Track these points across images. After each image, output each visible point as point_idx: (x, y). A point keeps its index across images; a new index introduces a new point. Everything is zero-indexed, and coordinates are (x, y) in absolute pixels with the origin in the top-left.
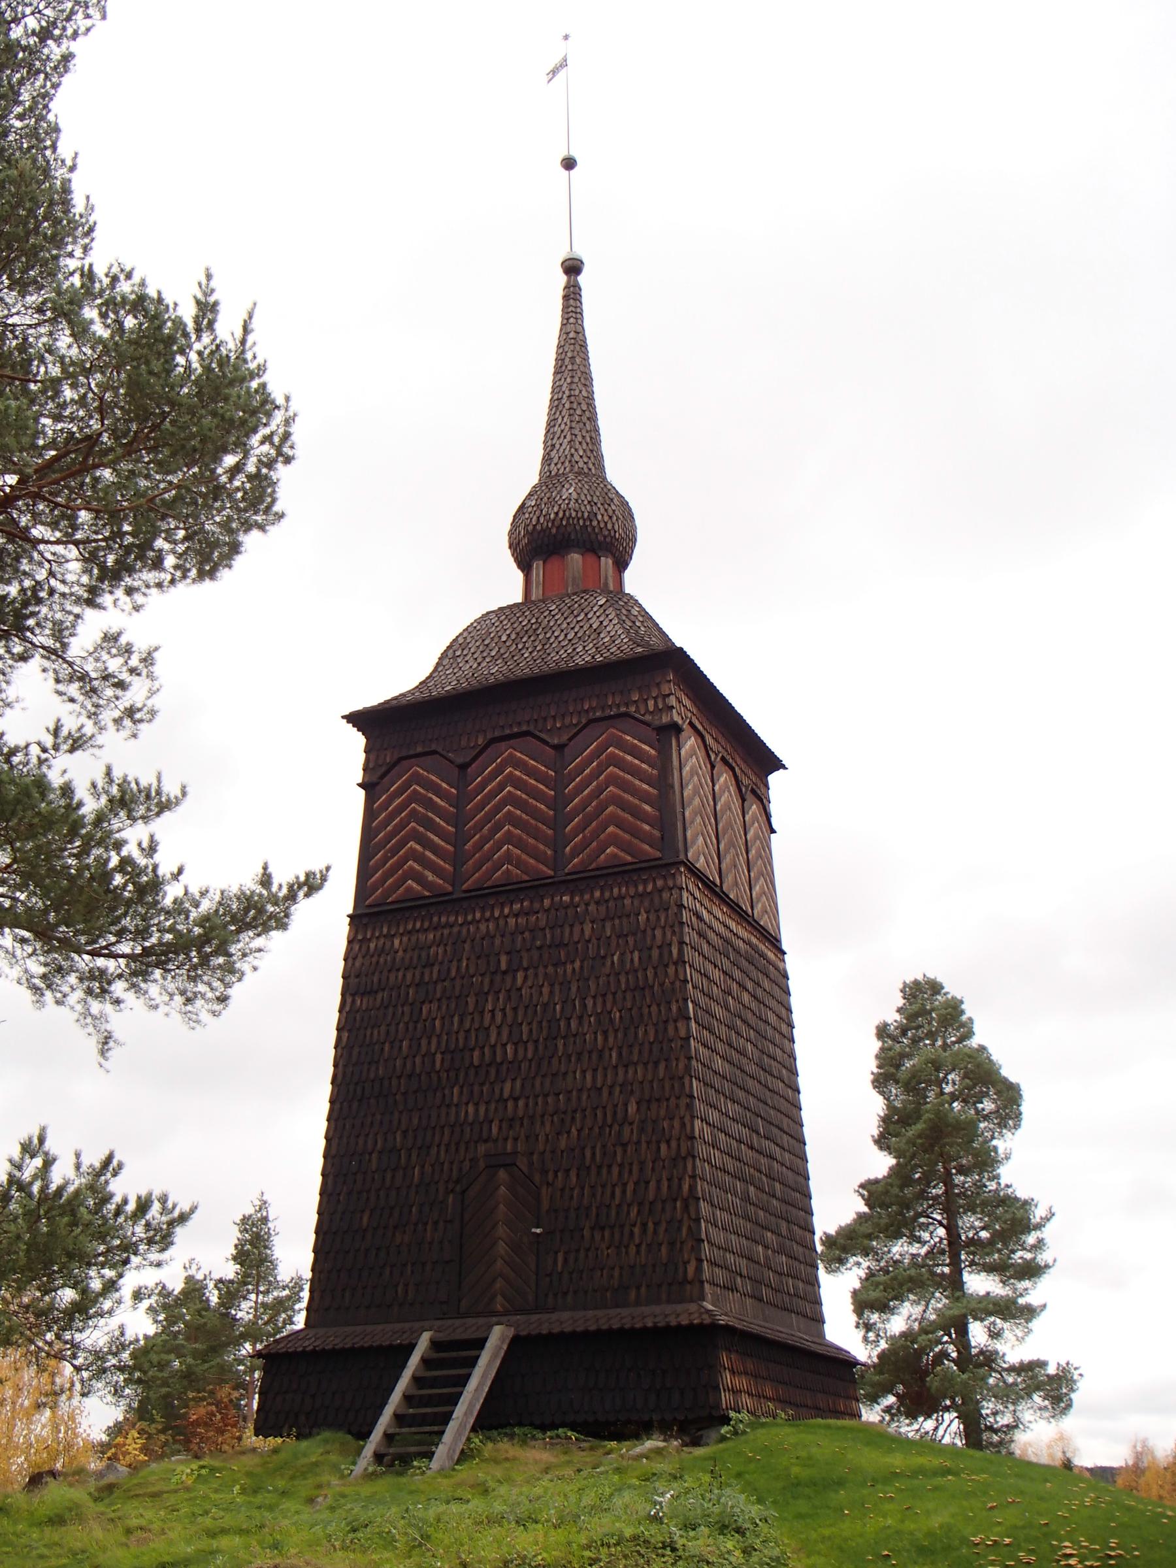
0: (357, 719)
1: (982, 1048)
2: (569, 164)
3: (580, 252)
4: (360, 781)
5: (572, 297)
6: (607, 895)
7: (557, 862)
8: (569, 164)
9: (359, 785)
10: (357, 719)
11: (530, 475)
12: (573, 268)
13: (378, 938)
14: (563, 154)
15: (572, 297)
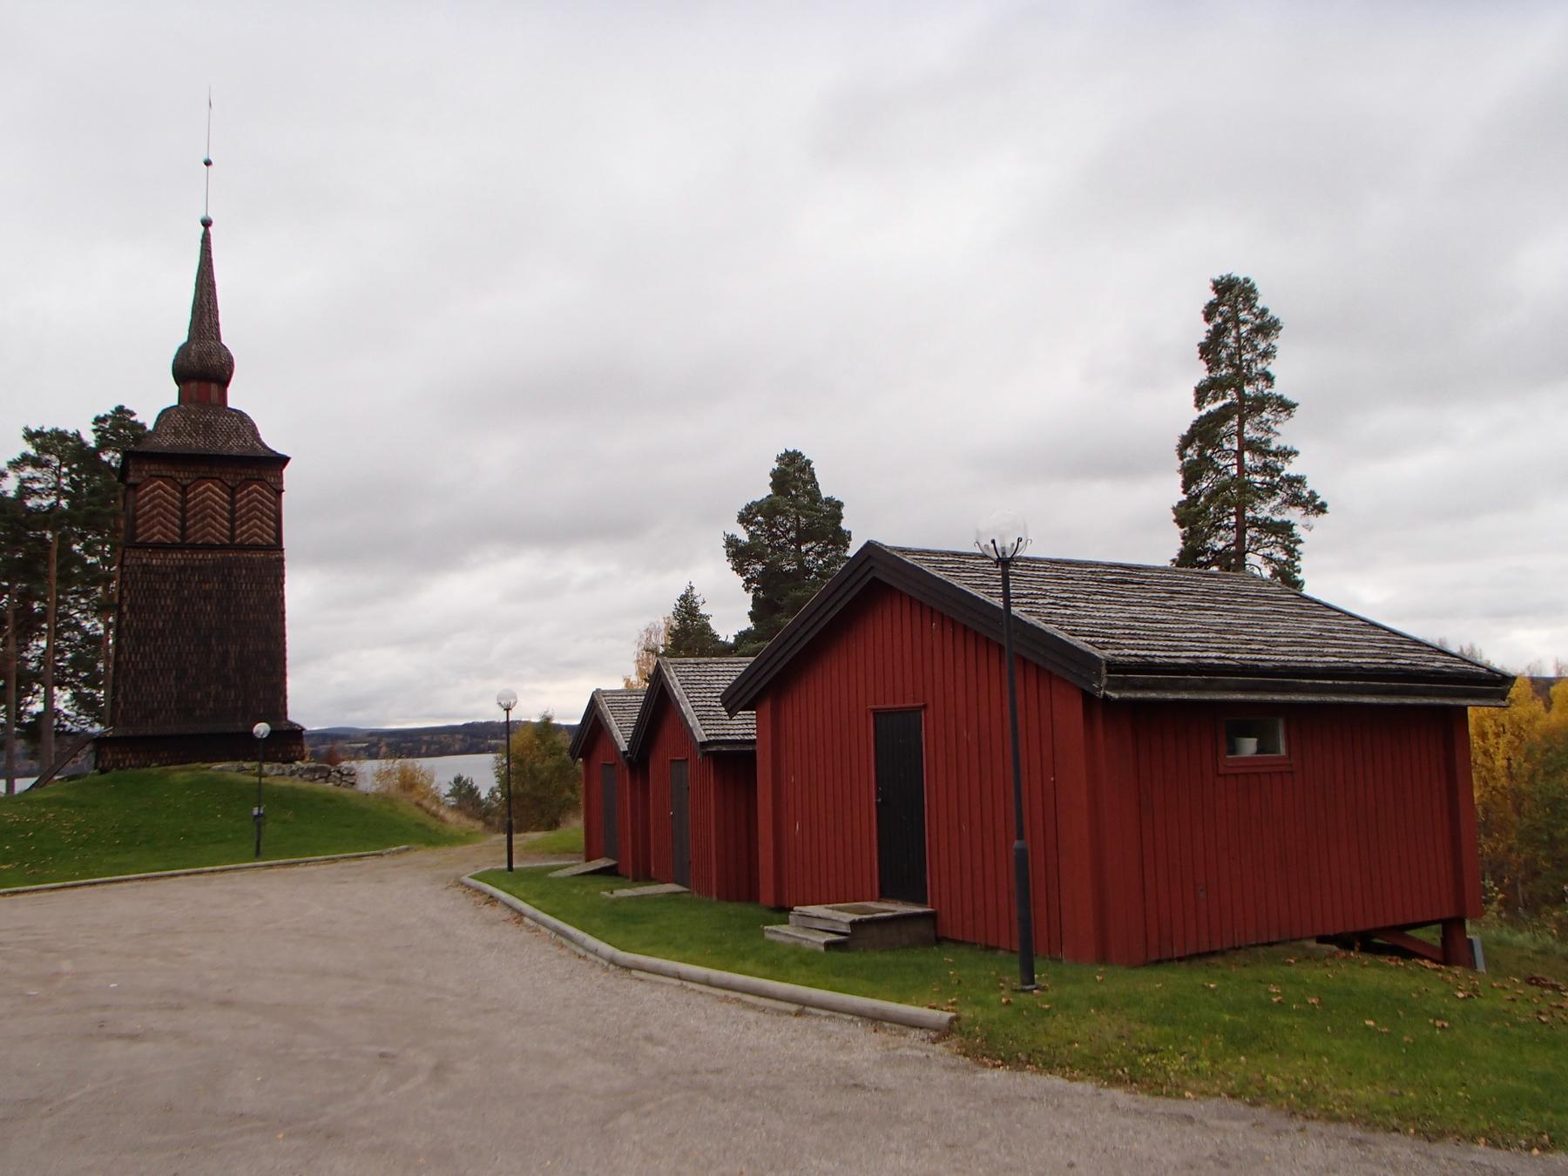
1: (871, 548)
2: (208, 163)
3: (211, 215)
5: (206, 241)
6: (139, 562)
7: (232, 537)
8: (208, 163)
12: (207, 224)
13: (132, 558)
14: (205, 157)
15: (206, 241)
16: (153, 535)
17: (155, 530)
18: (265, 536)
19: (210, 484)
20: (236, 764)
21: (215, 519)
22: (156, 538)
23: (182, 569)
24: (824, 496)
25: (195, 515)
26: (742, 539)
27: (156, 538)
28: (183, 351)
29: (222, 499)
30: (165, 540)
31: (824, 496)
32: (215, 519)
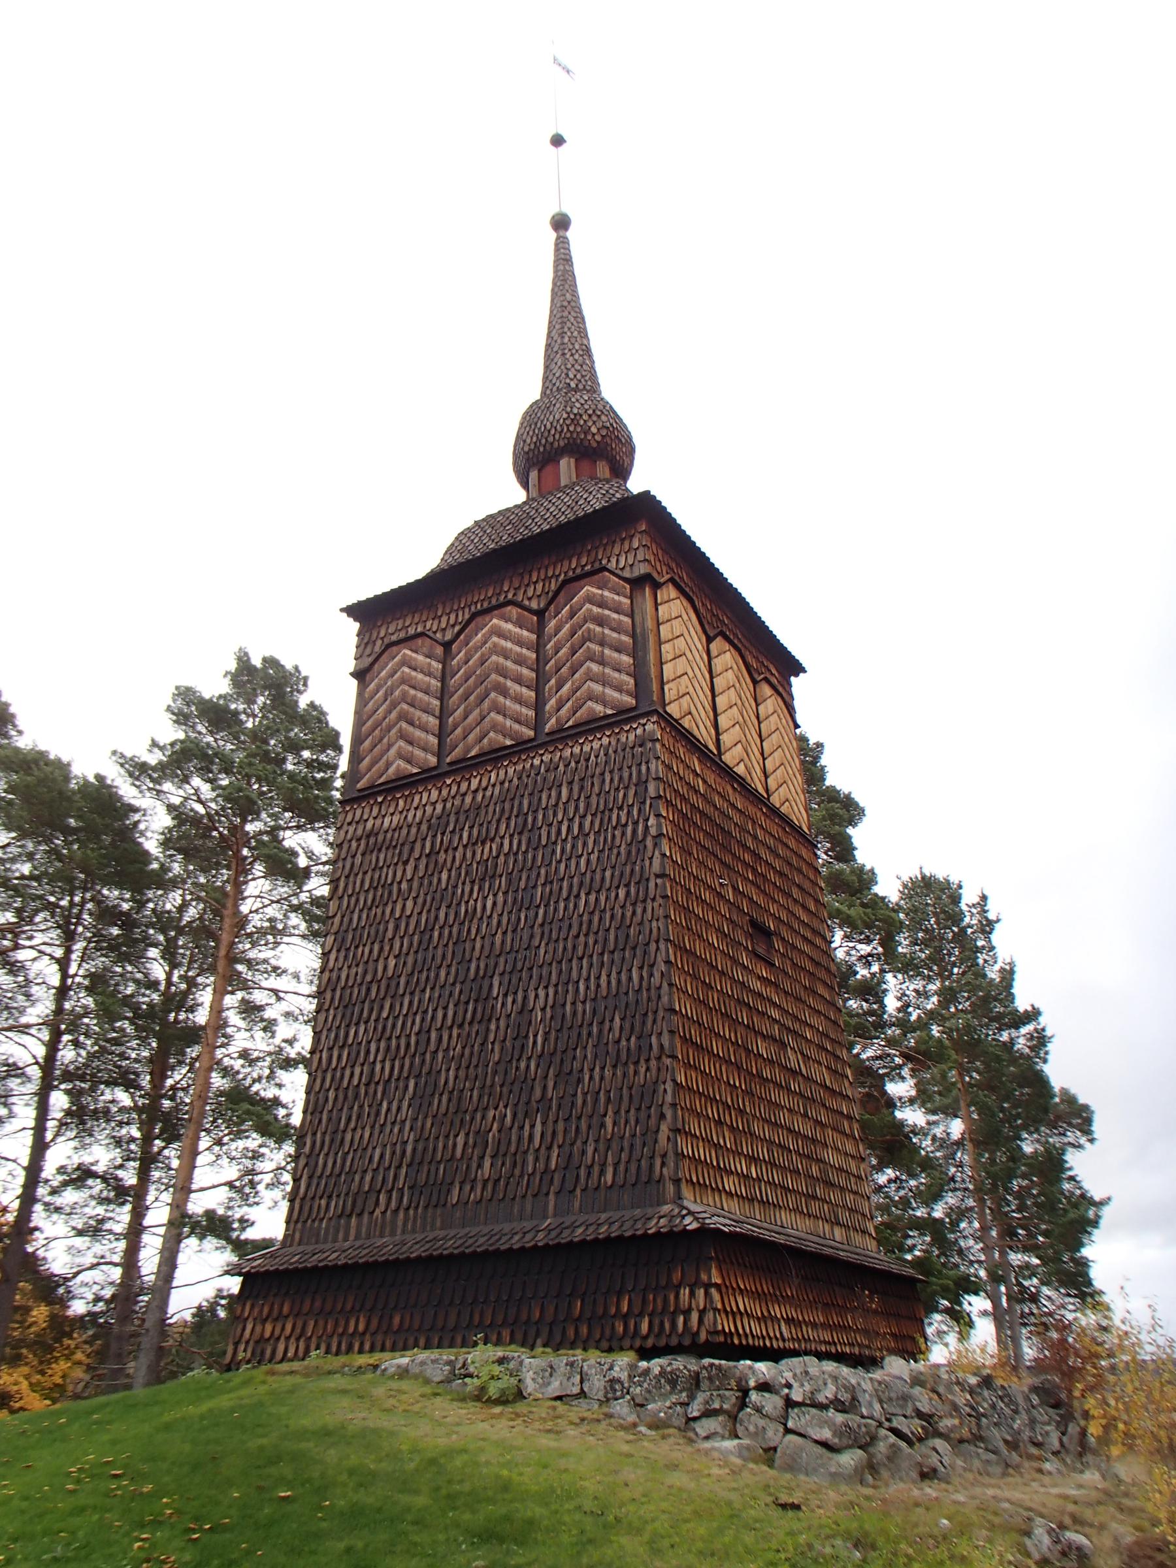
0: (355, 611)
2: (558, 141)
4: (352, 670)
8: (558, 141)
9: (352, 674)
10: (355, 611)
11: (533, 392)
12: (561, 223)
16: (388, 765)
17: (393, 752)
18: (609, 691)
19: (495, 621)
20: (447, 1355)
21: (504, 692)
22: (391, 770)
23: (438, 825)
24: (1086, 1252)
25: (466, 697)
26: (1111, 1296)
27: (391, 770)
28: (531, 418)
29: (519, 642)
30: (409, 767)
31: (1086, 1252)
32: (504, 692)
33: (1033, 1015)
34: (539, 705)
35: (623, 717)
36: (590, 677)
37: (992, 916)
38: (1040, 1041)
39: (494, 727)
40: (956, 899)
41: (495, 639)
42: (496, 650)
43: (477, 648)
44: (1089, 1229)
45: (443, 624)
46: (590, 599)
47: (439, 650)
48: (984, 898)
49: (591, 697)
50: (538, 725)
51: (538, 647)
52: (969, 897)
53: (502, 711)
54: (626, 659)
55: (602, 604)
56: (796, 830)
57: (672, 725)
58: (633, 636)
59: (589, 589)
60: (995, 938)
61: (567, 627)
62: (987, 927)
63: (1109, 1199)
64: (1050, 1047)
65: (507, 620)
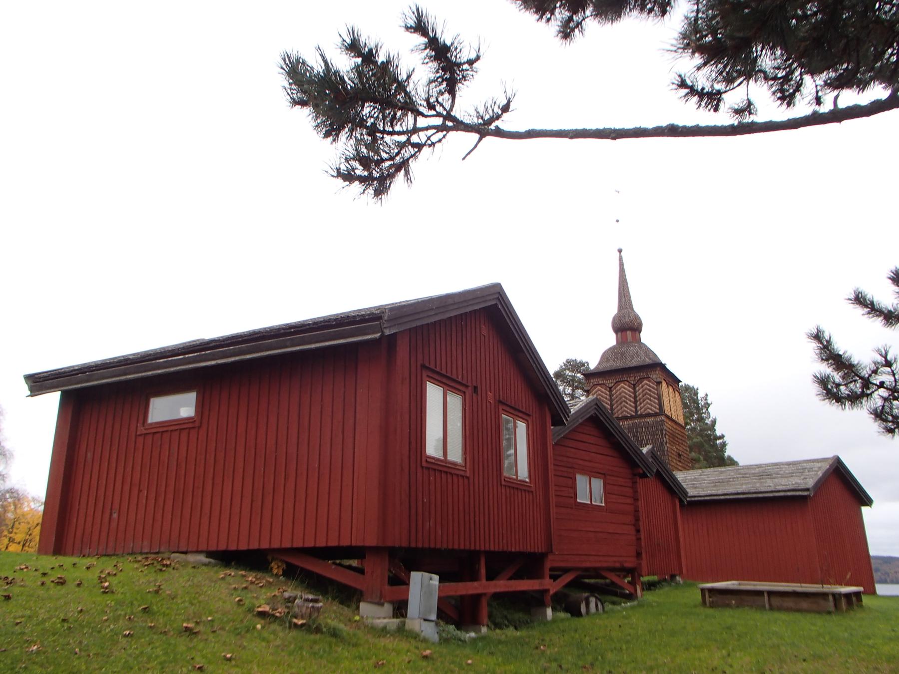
12: (620, 251)
29: (629, 391)
33: (722, 437)
34: (636, 408)
35: (656, 415)
36: (647, 403)
37: (709, 402)
38: (724, 445)
39: (625, 411)
40: (696, 394)
41: (623, 389)
42: (623, 392)
43: (618, 390)
44: (708, 421)
45: (610, 382)
46: (647, 384)
47: (608, 389)
48: (707, 395)
49: (649, 408)
50: (636, 411)
51: (635, 393)
52: (701, 395)
53: (626, 407)
54: (656, 401)
55: (650, 386)
56: (680, 425)
57: (667, 416)
58: (658, 395)
59: (646, 382)
60: (710, 409)
61: (641, 390)
62: (707, 405)
63: (817, 337)
64: (727, 447)
65: (626, 385)
